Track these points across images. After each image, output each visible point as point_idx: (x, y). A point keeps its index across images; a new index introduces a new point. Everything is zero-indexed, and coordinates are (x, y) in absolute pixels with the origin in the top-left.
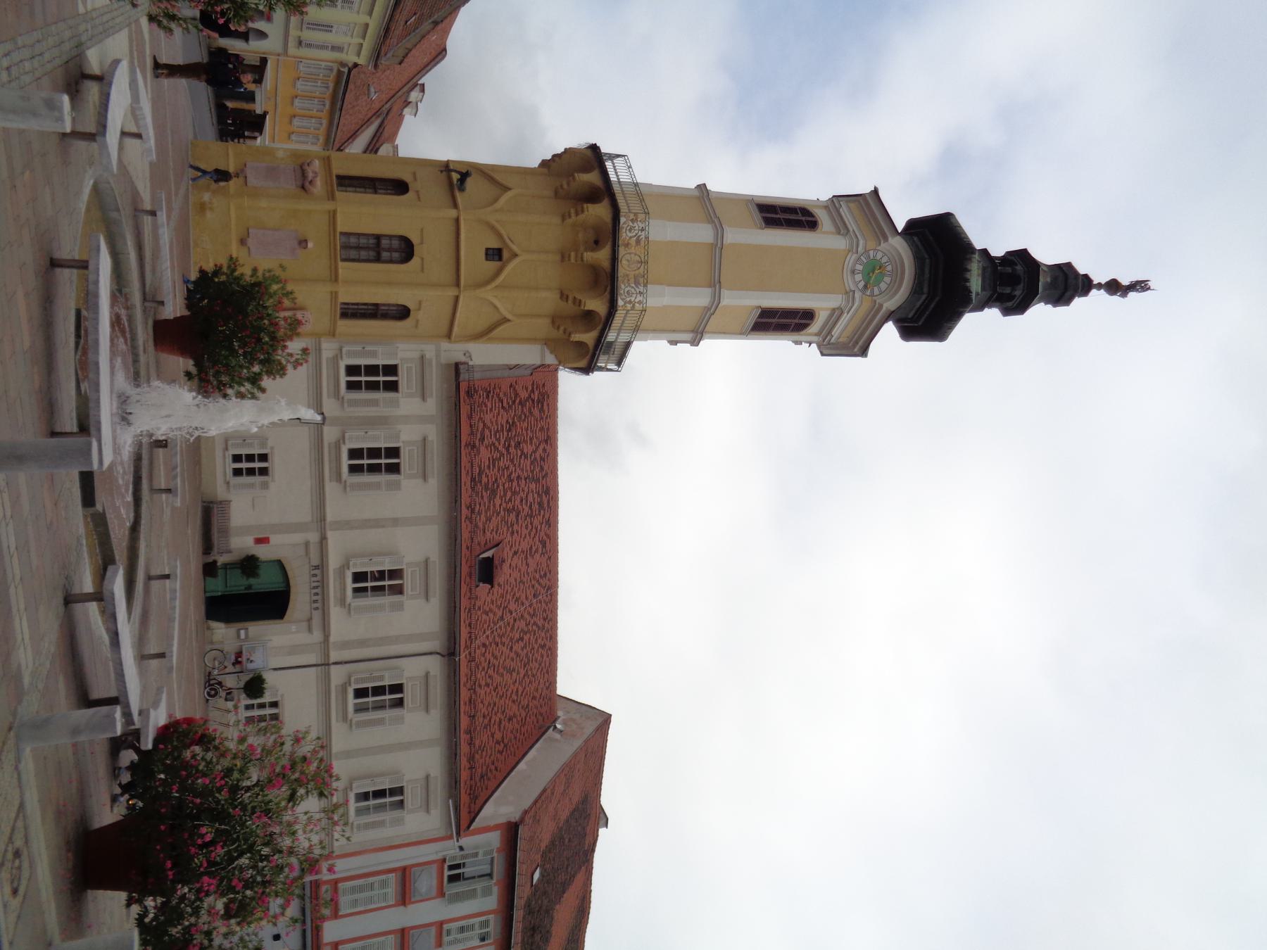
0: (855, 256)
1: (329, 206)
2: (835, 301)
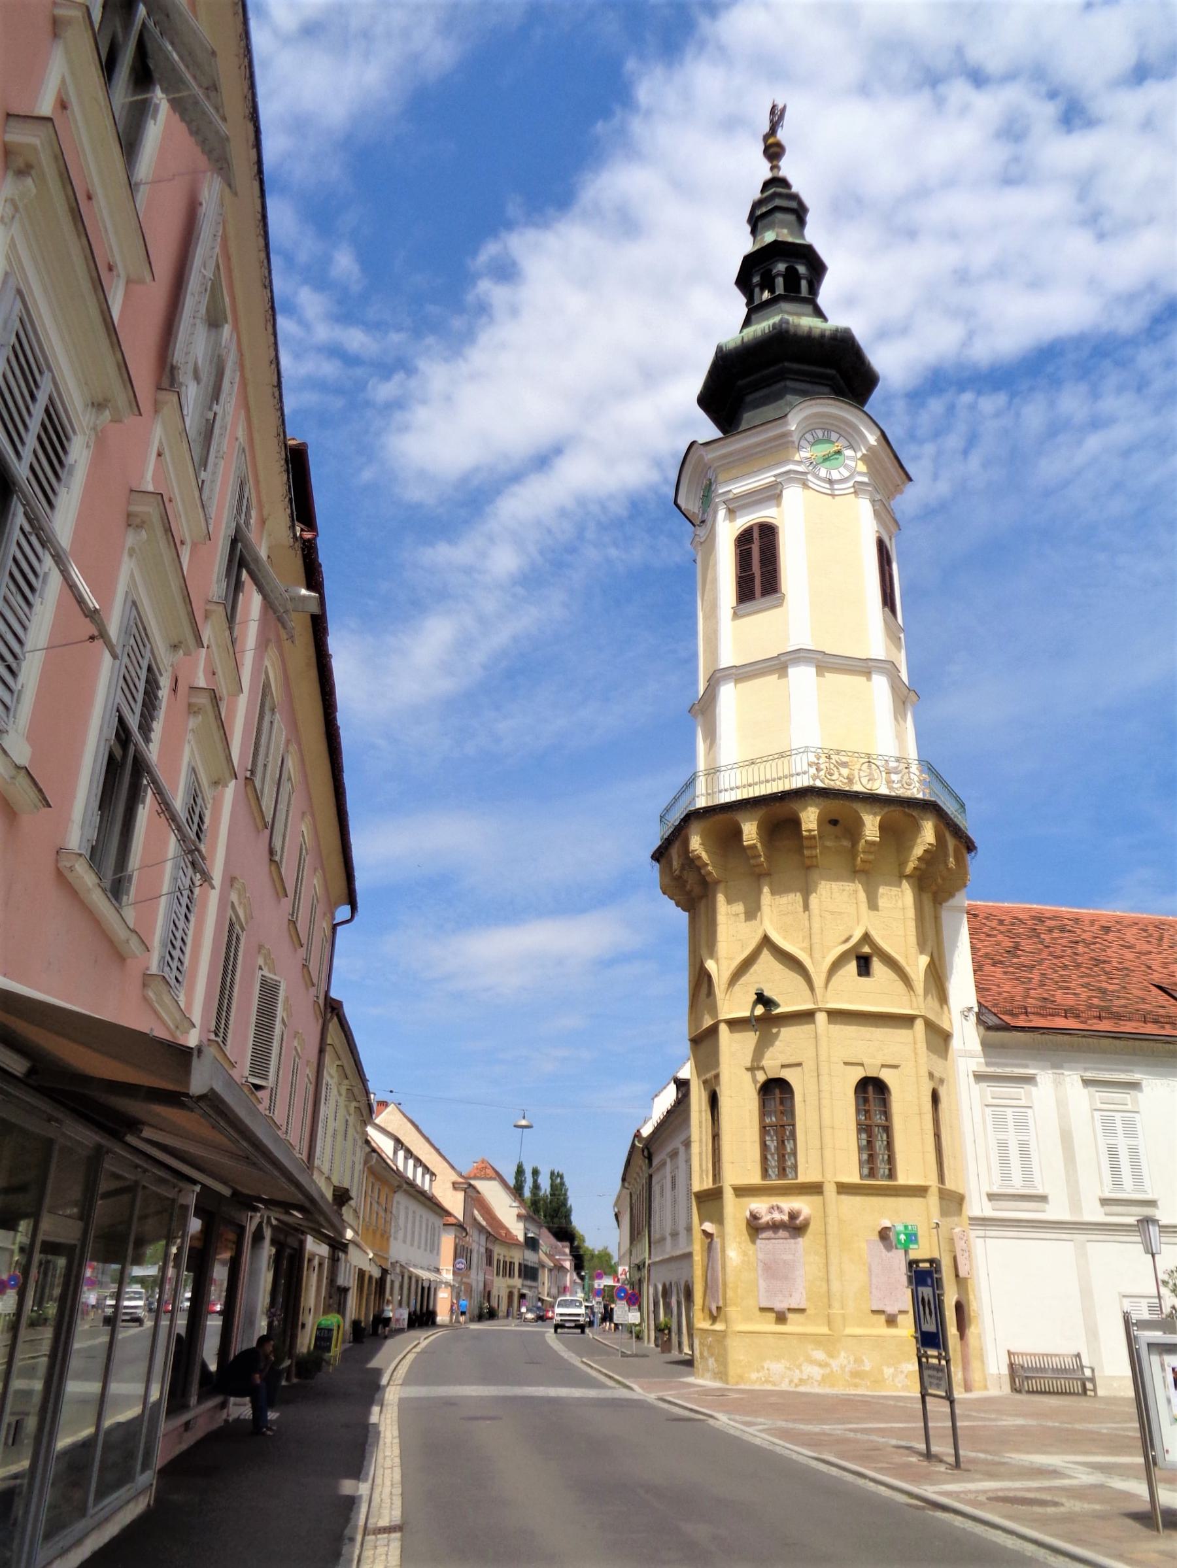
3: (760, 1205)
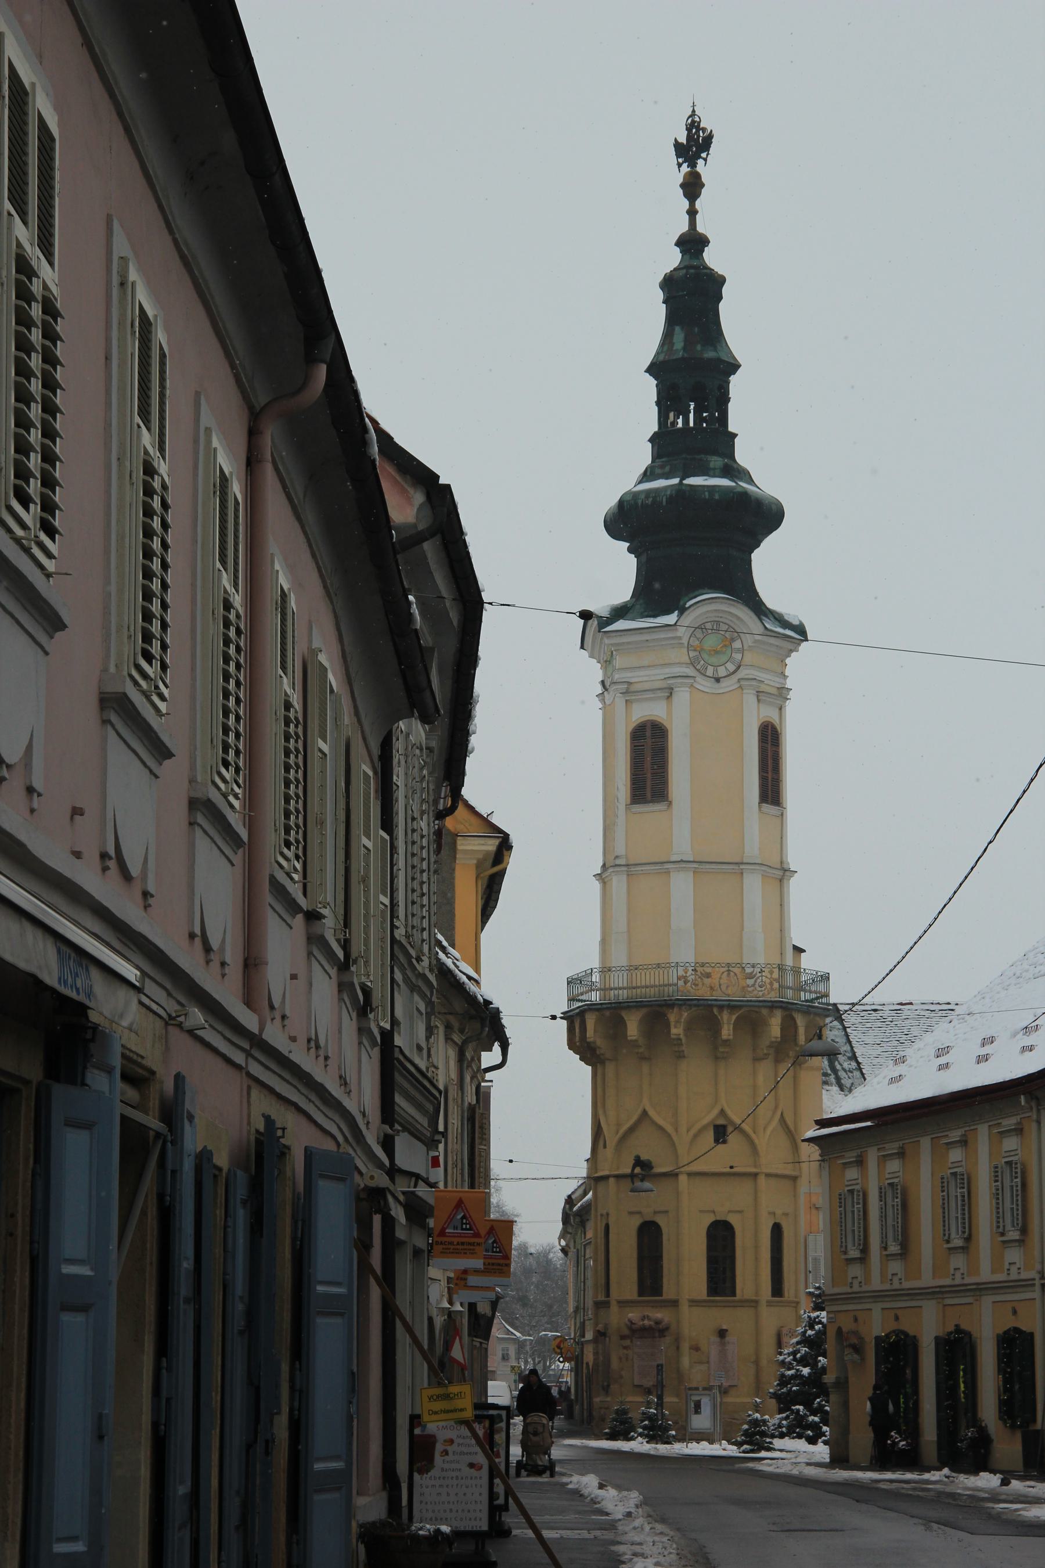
0: (700, 679)
1: (685, 1308)
2: (750, 699)
3: (634, 1315)
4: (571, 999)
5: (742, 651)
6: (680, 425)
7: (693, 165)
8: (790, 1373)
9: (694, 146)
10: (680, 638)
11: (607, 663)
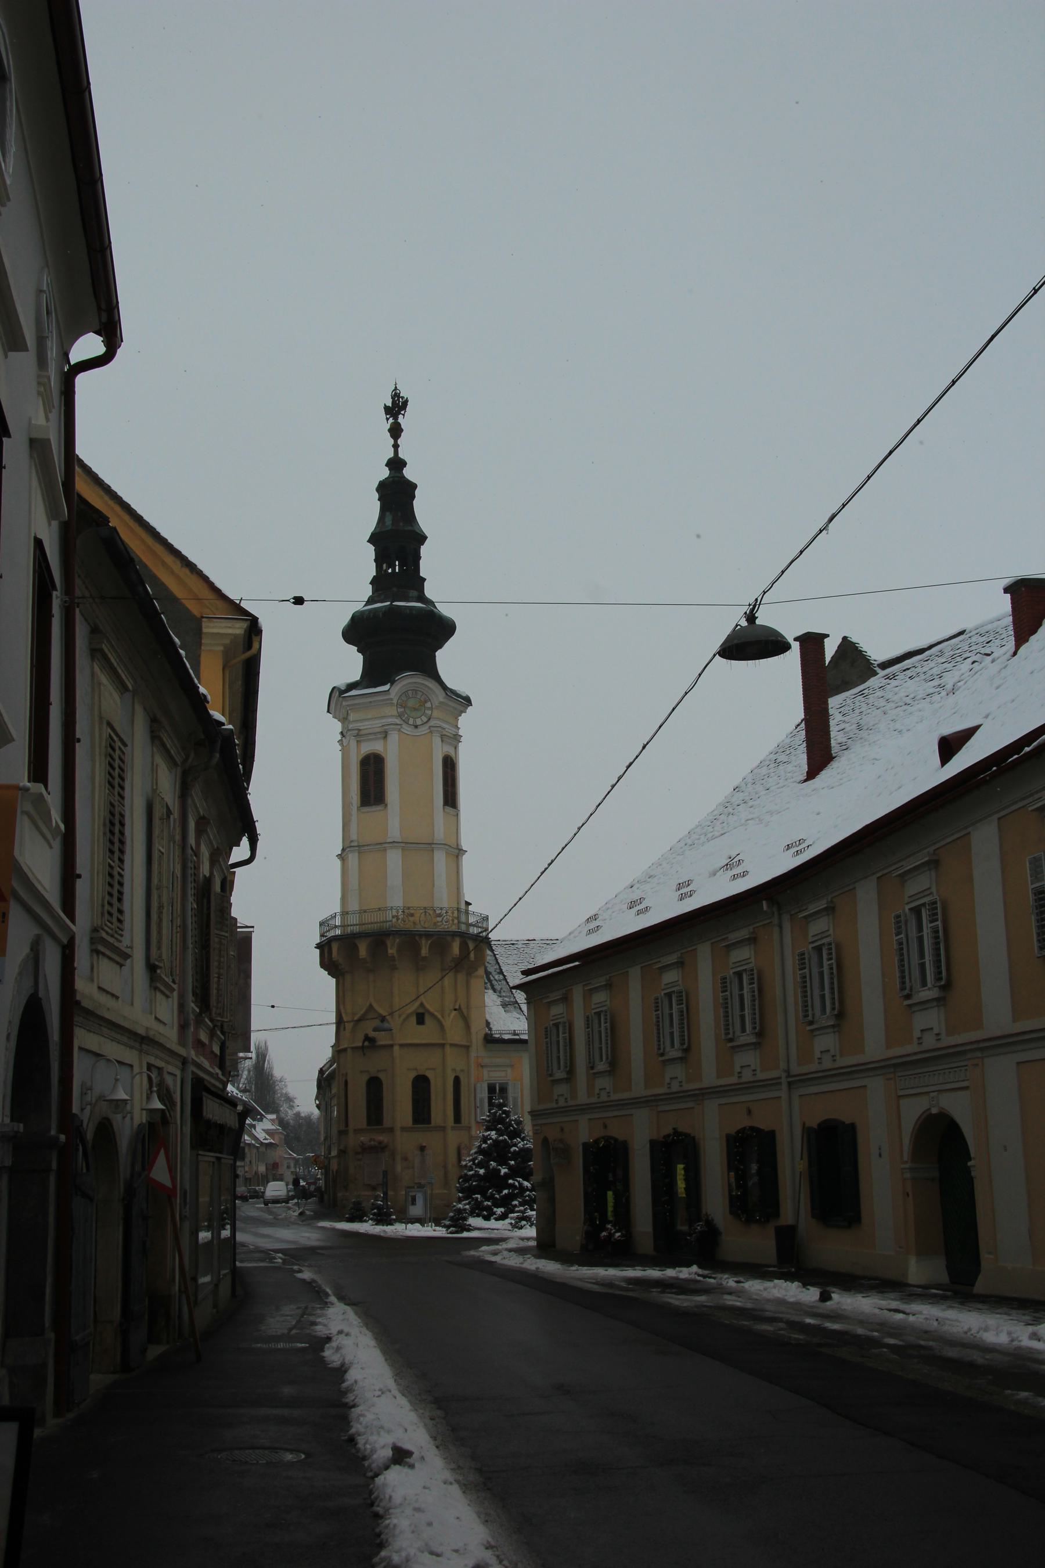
0: (404, 726)
1: (398, 1133)
2: (437, 740)
4: (322, 935)
5: (431, 709)
6: (390, 571)
7: (396, 418)
8: (471, 1173)
9: (397, 407)
10: (392, 699)
11: (344, 720)
